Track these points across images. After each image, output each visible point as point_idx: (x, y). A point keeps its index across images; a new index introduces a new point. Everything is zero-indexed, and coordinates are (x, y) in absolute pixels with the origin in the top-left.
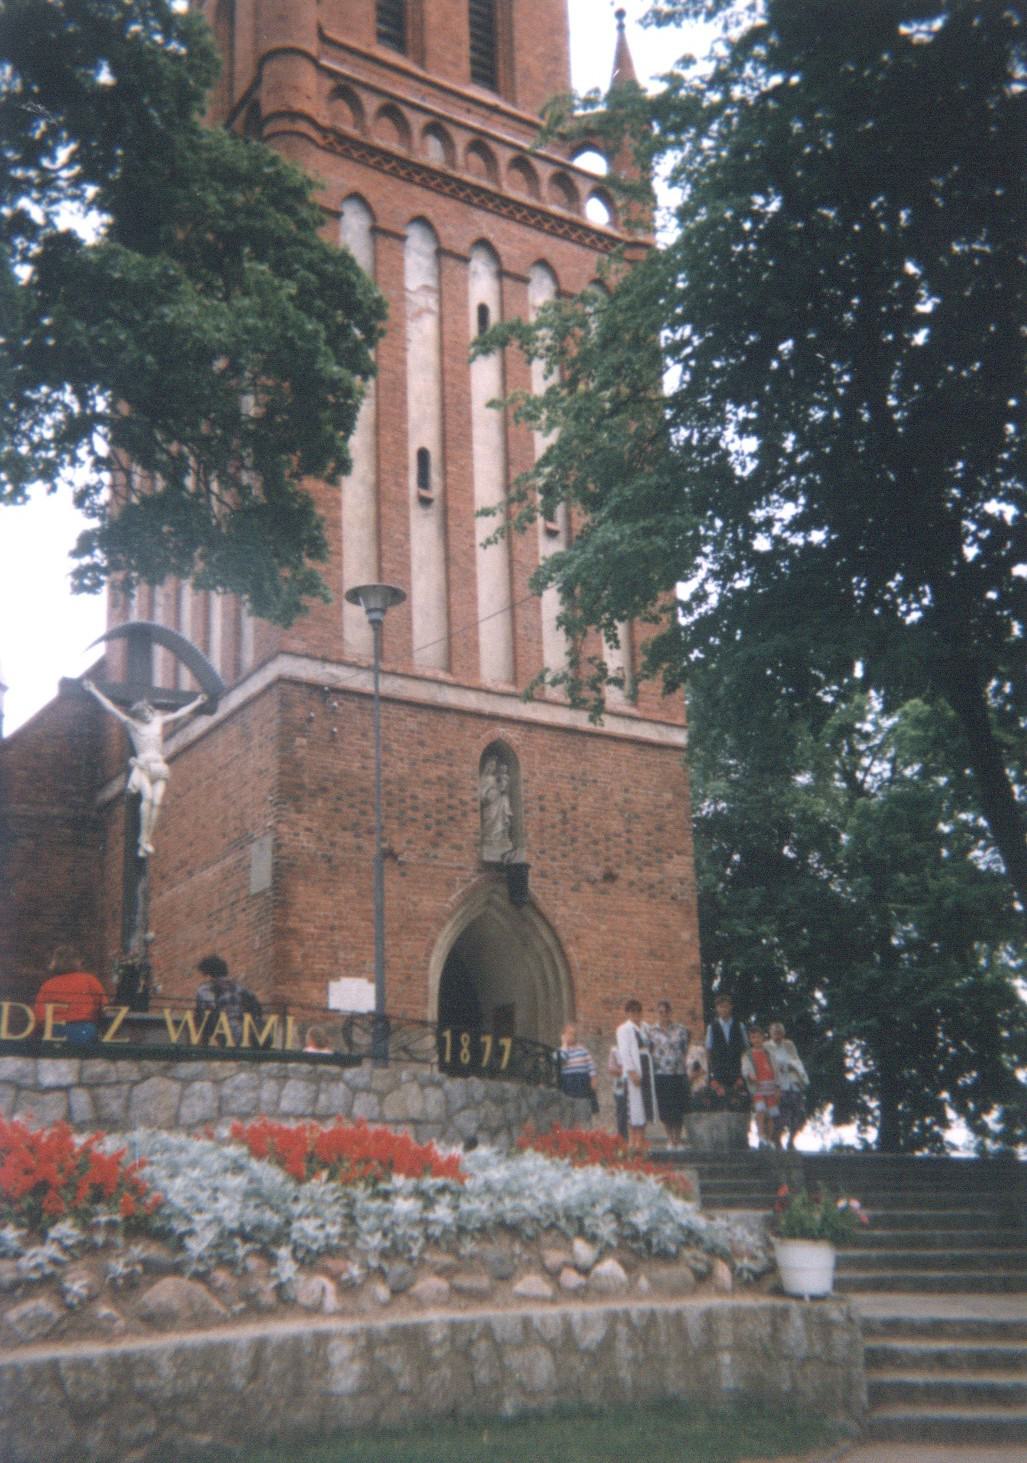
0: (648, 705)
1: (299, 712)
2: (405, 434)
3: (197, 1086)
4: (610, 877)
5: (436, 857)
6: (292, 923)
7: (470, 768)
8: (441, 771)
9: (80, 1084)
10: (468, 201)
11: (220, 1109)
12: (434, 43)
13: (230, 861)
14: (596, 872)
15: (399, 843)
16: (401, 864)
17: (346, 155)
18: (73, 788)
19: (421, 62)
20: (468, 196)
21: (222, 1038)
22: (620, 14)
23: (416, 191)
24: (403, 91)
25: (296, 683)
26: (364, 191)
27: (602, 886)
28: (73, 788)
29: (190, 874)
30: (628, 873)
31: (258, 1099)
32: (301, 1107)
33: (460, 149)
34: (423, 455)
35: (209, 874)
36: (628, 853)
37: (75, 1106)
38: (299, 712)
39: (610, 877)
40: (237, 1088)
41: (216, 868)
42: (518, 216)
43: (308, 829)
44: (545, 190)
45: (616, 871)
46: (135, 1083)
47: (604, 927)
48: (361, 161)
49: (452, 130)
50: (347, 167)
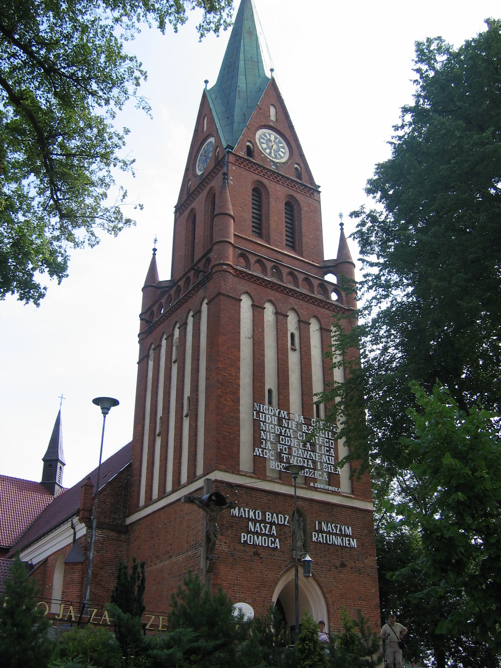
0: (358, 494)
2: (264, 383)
4: (343, 565)
5: (274, 555)
10: (287, 294)
12: (273, 235)
13: (190, 553)
14: (338, 563)
16: (261, 558)
17: (243, 278)
19: (268, 242)
20: (318, 303)
24: (263, 253)
25: (222, 482)
29: (171, 557)
33: (284, 275)
34: (270, 391)
35: (180, 558)
39: (343, 565)
41: (184, 556)
42: (269, 286)
43: (225, 543)
44: (269, 272)
45: (346, 563)
47: (341, 587)
48: (249, 280)
49: (250, 256)
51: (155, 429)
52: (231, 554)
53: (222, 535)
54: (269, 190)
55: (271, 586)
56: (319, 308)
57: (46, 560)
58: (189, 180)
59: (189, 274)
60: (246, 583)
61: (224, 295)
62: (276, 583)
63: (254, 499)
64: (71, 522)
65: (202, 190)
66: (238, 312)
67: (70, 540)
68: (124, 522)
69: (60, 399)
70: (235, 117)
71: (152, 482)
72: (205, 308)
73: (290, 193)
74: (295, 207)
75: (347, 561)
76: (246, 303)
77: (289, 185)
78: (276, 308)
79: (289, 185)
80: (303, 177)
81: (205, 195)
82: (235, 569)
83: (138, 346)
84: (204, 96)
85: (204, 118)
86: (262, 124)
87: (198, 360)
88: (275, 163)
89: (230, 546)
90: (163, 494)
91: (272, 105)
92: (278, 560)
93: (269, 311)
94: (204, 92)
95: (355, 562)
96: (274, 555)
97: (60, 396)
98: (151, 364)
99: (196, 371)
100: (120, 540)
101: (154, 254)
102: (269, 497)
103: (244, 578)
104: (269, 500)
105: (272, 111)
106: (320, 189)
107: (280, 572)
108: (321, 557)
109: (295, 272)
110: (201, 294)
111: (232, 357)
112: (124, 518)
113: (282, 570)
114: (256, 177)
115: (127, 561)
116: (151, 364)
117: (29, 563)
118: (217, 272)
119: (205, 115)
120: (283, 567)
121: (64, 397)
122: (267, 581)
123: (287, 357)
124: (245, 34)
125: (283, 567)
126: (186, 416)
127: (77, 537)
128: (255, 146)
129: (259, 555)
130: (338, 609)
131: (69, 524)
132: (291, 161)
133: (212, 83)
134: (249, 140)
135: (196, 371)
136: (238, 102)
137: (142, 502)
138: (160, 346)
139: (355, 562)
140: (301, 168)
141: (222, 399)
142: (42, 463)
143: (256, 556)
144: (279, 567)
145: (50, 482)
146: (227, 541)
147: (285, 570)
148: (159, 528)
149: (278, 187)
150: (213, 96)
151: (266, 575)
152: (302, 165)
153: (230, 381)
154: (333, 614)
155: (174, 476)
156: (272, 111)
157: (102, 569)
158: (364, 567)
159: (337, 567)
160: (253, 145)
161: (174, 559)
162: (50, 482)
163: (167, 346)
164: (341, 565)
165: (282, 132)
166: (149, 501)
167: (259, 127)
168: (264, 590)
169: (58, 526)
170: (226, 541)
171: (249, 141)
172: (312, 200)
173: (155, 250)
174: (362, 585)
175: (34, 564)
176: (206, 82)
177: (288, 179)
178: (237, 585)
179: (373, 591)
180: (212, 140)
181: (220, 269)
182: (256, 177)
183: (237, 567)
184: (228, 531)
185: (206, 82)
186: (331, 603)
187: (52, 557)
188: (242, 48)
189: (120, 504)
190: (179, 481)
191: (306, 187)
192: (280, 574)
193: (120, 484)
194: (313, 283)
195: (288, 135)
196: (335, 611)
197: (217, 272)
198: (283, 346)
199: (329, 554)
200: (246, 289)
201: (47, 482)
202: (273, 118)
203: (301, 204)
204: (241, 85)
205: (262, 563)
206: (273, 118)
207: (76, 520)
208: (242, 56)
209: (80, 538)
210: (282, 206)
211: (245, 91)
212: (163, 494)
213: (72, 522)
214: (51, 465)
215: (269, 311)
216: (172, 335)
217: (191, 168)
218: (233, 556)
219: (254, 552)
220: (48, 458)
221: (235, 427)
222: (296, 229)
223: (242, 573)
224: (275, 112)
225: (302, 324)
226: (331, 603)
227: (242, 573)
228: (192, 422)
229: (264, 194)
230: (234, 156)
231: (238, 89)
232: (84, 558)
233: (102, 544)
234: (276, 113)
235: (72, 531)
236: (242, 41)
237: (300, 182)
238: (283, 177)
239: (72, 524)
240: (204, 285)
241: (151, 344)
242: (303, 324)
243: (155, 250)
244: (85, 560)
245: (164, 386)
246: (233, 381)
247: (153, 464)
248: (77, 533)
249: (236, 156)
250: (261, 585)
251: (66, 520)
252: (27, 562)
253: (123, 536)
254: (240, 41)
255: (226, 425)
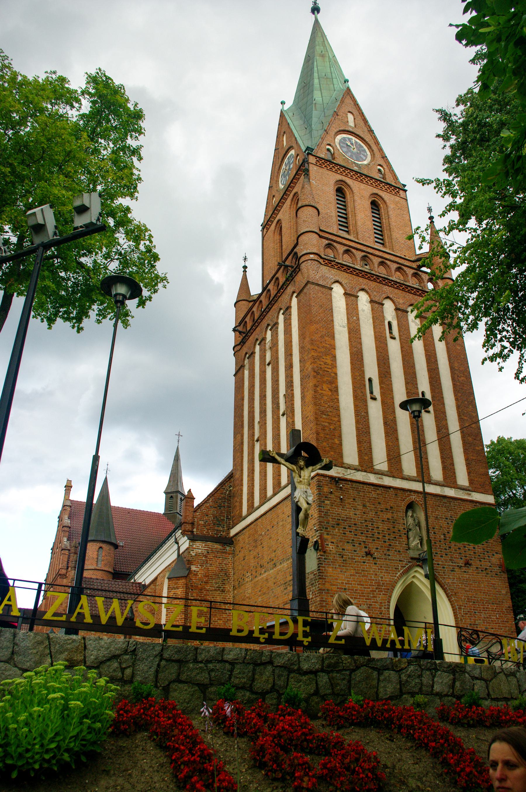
1: (326, 489)
3: (386, 673)
4: (467, 564)
5: (389, 555)
6: (327, 586)
7: (401, 514)
8: (389, 515)
9: (322, 670)
11: (401, 689)
14: (461, 563)
15: (372, 547)
16: (374, 558)
18: (221, 529)
21: (81, 616)
22: (430, 210)
23: (361, 280)
26: (340, 280)
27: (464, 569)
28: (221, 529)
29: (275, 565)
30: (475, 563)
31: (422, 684)
32: (446, 690)
36: (474, 553)
37: (321, 684)
38: (326, 489)
39: (467, 564)
40: (409, 676)
42: (354, 177)
43: (332, 542)
45: (471, 562)
46: (353, 670)
50: (334, 271)
51: (253, 435)
52: (340, 555)
53: (328, 534)
54: (353, 189)
55: (388, 589)
56: (416, 297)
57: (156, 579)
58: (274, 196)
59: (277, 275)
60: (359, 586)
61: (313, 283)
62: (394, 587)
63: (361, 494)
64: (174, 537)
65: (286, 199)
66: (330, 300)
67: (175, 556)
68: (229, 533)
69: (177, 437)
70: (313, 126)
71: (253, 489)
72: (294, 301)
73: (374, 192)
74: (381, 205)
75: (471, 560)
76: (338, 291)
77: (373, 184)
78: (370, 296)
79: (373, 184)
80: (387, 177)
81: (289, 203)
82: (345, 572)
83: (233, 359)
84: (282, 115)
85: (283, 136)
86: (341, 129)
87: (291, 355)
88: (357, 165)
89: (337, 546)
90: (264, 499)
91: (350, 112)
92: (394, 560)
93: (363, 298)
94: (281, 112)
95: (480, 561)
96: (389, 555)
97: (177, 434)
98: (246, 373)
99: (289, 367)
100: (226, 553)
101: (245, 271)
102: (378, 492)
103: (357, 581)
104: (378, 494)
105: (350, 117)
106: (406, 188)
107: (397, 574)
108: (442, 556)
109: (387, 261)
110: (290, 289)
111: (325, 345)
112: (228, 530)
113: (399, 571)
114: (339, 177)
115: (234, 574)
116: (246, 373)
117: (143, 583)
118: (303, 262)
119: (284, 133)
120: (400, 568)
121: (181, 434)
122: (383, 584)
123: (386, 345)
124: (317, 57)
125: (400, 568)
126: (283, 415)
127: (181, 551)
128: (335, 148)
129: (372, 556)
130: (466, 614)
131: (172, 540)
132: (373, 162)
133: (289, 104)
134: (328, 143)
135: (289, 367)
136: (315, 113)
137: (245, 512)
138: (253, 353)
139: (480, 561)
140: (384, 169)
141: (318, 389)
142: (164, 496)
143: (369, 556)
144: (396, 568)
145: (171, 512)
146: (334, 541)
147: (402, 571)
148: (261, 535)
149: (363, 186)
150: (291, 114)
151: (382, 578)
152: (385, 167)
153: (326, 369)
154: (461, 620)
155: (274, 478)
156: (350, 117)
157: (208, 583)
158: (490, 566)
159: (461, 566)
160: (333, 148)
161: (279, 567)
162: (171, 512)
163: (260, 350)
164: (465, 564)
165: (362, 136)
166: (252, 509)
167: (338, 132)
168: (380, 594)
169: (164, 542)
170: (333, 541)
171: (329, 145)
172: (398, 198)
173: (245, 267)
174: (491, 586)
175: (147, 584)
176: (283, 103)
177: (372, 178)
178: (349, 590)
179: (504, 592)
180: (292, 152)
181: (306, 259)
182: (339, 177)
183: (347, 569)
184: (335, 530)
185: (283, 103)
186: (457, 607)
187: (161, 575)
188: (315, 69)
189: (224, 516)
190: (279, 483)
191: (391, 185)
192: (397, 575)
193: (222, 495)
194: (407, 272)
195: (368, 138)
196: (462, 616)
197: (303, 262)
198: (380, 334)
199: (451, 552)
200: (337, 278)
201: (169, 512)
202: (351, 123)
203: (388, 202)
204: (316, 99)
205: (375, 564)
206: (351, 123)
207: (179, 533)
208: (316, 75)
209: (183, 553)
210: (367, 204)
211: (321, 103)
212: (264, 499)
213: (175, 537)
214: (172, 497)
215: (363, 298)
216: (264, 339)
217: (274, 186)
218: (342, 557)
219: (366, 552)
220: (169, 491)
221: (335, 417)
222: (385, 225)
223: (353, 575)
224: (353, 119)
225: (399, 312)
226: (457, 607)
227: (353, 575)
228: (289, 419)
229: (348, 193)
230: (314, 158)
231: (314, 102)
232: (187, 572)
233: (206, 557)
234: (354, 119)
235: (176, 546)
236: (315, 63)
237: (385, 181)
238: (367, 176)
239: (176, 539)
240: (292, 280)
241: (246, 353)
242: (401, 312)
243: (245, 267)
244: (188, 574)
245: (260, 390)
246: (330, 371)
247: (253, 470)
248: (181, 548)
249: (317, 157)
250: (376, 588)
251: (170, 535)
252: (141, 583)
253: (228, 548)
254: (313, 63)
255: (325, 415)
